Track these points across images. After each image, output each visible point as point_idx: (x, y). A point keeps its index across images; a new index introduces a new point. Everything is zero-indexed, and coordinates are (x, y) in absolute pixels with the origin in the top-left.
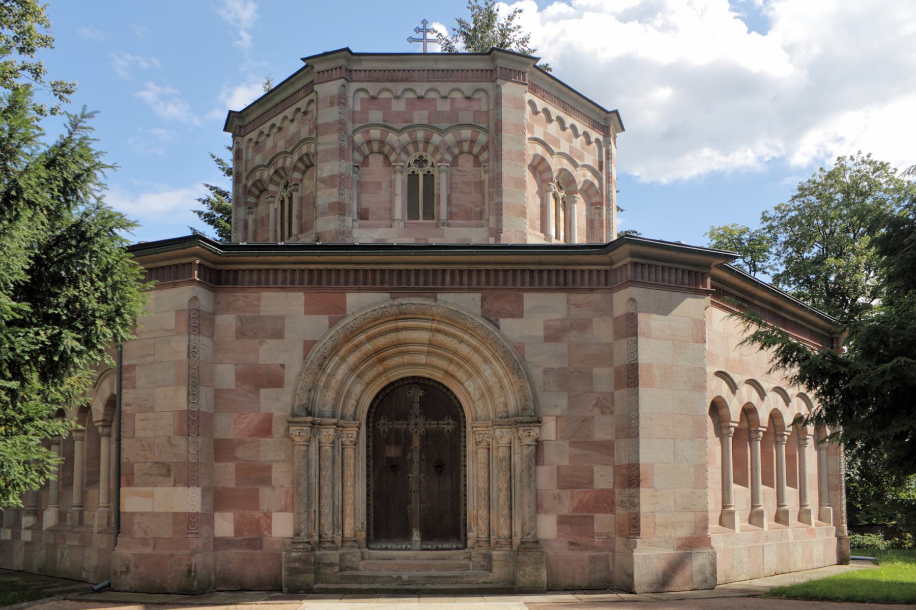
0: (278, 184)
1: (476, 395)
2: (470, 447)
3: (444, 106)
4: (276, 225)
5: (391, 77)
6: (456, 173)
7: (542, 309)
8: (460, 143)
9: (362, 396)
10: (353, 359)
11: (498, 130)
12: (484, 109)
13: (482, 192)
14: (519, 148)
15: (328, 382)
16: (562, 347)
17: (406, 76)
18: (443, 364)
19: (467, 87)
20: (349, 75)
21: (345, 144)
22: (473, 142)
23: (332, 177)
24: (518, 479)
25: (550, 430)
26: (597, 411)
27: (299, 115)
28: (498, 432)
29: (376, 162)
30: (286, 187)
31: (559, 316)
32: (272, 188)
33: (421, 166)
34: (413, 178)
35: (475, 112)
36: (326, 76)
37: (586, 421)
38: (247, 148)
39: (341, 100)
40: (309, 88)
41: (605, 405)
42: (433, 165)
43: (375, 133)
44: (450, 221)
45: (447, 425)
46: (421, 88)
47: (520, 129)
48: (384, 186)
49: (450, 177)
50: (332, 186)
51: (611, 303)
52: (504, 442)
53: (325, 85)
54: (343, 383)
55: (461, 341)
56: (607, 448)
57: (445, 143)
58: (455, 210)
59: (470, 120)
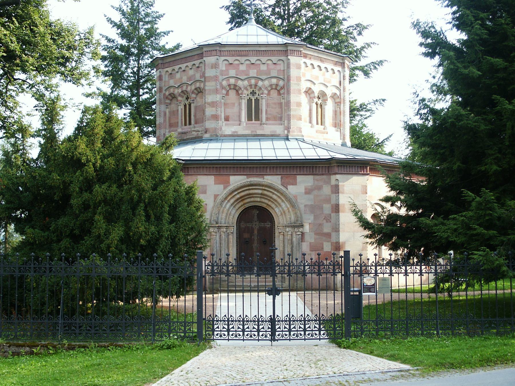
0: (183, 97)
1: (279, 214)
2: (277, 234)
3: (264, 68)
4: (182, 117)
5: (240, 54)
6: (269, 98)
7: (305, 181)
8: (271, 85)
9: (235, 214)
10: (232, 201)
11: (289, 80)
12: (282, 69)
13: (281, 108)
14: (298, 87)
15: (223, 210)
16: (311, 196)
17: (246, 54)
18: (266, 201)
19: (275, 59)
20: (220, 53)
21: (219, 87)
22: (277, 85)
23: (213, 102)
24: (295, 247)
25: (307, 228)
26: (325, 221)
27: (194, 67)
28: (287, 229)
29: (232, 93)
30: (187, 98)
31: (310, 184)
32: (180, 98)
33: (253, 95)
34: (249, 101)
35: (278, 71)
36: (210, 53)
37: (321, 225)
38: (165, 75)
39: (215, 66)
40: (201, 56)
41: (328, 219)
42: (259, 95)
43: (232, 81)
44: (267, 122)
45: (268, 225)
46: (253, 59)
47: (299, 79)
48: (236, 105)
49: (267, 101)
50: (213, 107)
51: (330, 179)
52: (290, 233)
53: (209, 58)
54: (228, 210)
55: (273, 193)
56: (328, 235)
57: (265, 86)
58: (269, 116)
59: (276, 75)
